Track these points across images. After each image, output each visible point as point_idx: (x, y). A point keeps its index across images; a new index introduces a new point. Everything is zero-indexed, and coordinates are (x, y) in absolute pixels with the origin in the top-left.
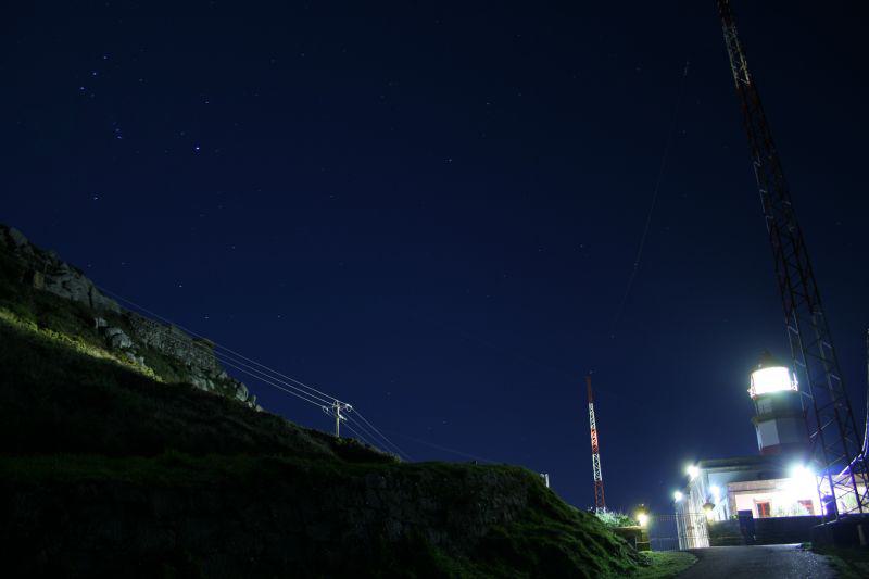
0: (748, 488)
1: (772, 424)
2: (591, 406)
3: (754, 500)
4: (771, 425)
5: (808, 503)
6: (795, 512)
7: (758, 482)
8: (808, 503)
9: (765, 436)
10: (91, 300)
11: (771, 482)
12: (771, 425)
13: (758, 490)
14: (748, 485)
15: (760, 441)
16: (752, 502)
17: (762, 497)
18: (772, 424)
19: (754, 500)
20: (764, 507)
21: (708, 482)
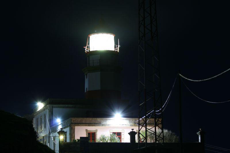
0: (84, 122)
1: (98, 74)
2: (200, 141)
3: (87, 130)
4: (97, 75)
5: (119, 134)
6: (123, 139)
7: (91, 119)
8: (119, 134)
9: (90, 83)
10: (148, 8)
11: (99, 120)
12: (97, 75)
13: (90, 124)
14: (85, 120)
15: (86, 86)
16: (85, 133)
17: (91, 129)
18: (98, 74)
19: (87, 130)
20: (93, 135)
21: (52, 113)
